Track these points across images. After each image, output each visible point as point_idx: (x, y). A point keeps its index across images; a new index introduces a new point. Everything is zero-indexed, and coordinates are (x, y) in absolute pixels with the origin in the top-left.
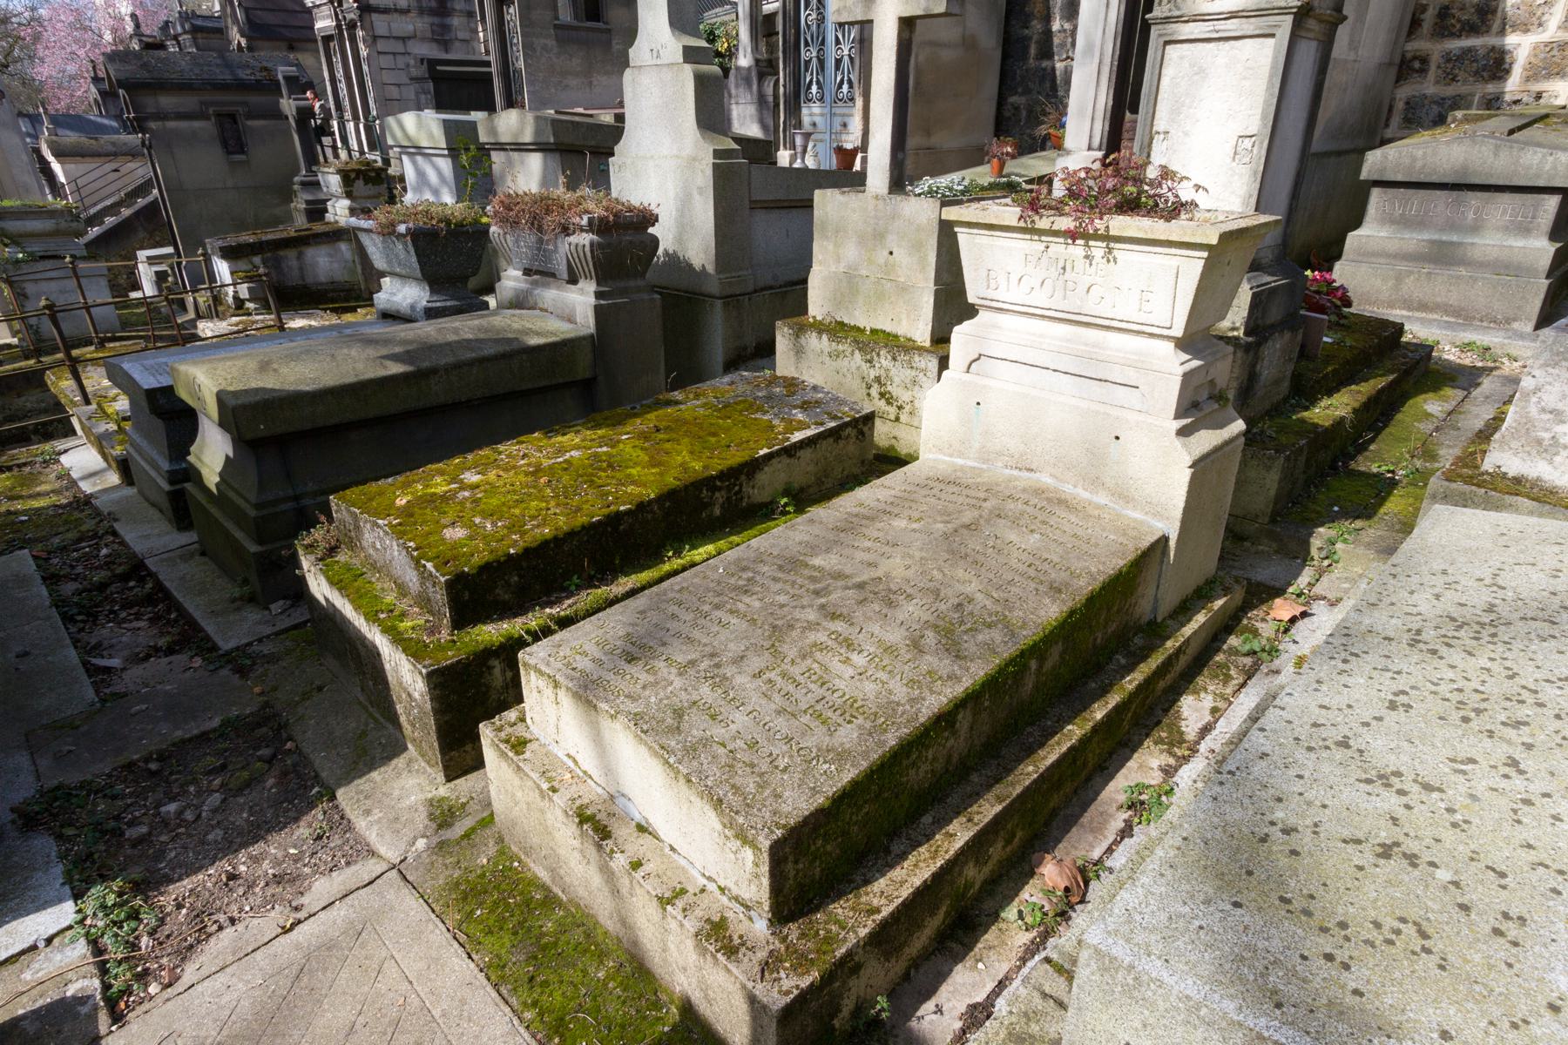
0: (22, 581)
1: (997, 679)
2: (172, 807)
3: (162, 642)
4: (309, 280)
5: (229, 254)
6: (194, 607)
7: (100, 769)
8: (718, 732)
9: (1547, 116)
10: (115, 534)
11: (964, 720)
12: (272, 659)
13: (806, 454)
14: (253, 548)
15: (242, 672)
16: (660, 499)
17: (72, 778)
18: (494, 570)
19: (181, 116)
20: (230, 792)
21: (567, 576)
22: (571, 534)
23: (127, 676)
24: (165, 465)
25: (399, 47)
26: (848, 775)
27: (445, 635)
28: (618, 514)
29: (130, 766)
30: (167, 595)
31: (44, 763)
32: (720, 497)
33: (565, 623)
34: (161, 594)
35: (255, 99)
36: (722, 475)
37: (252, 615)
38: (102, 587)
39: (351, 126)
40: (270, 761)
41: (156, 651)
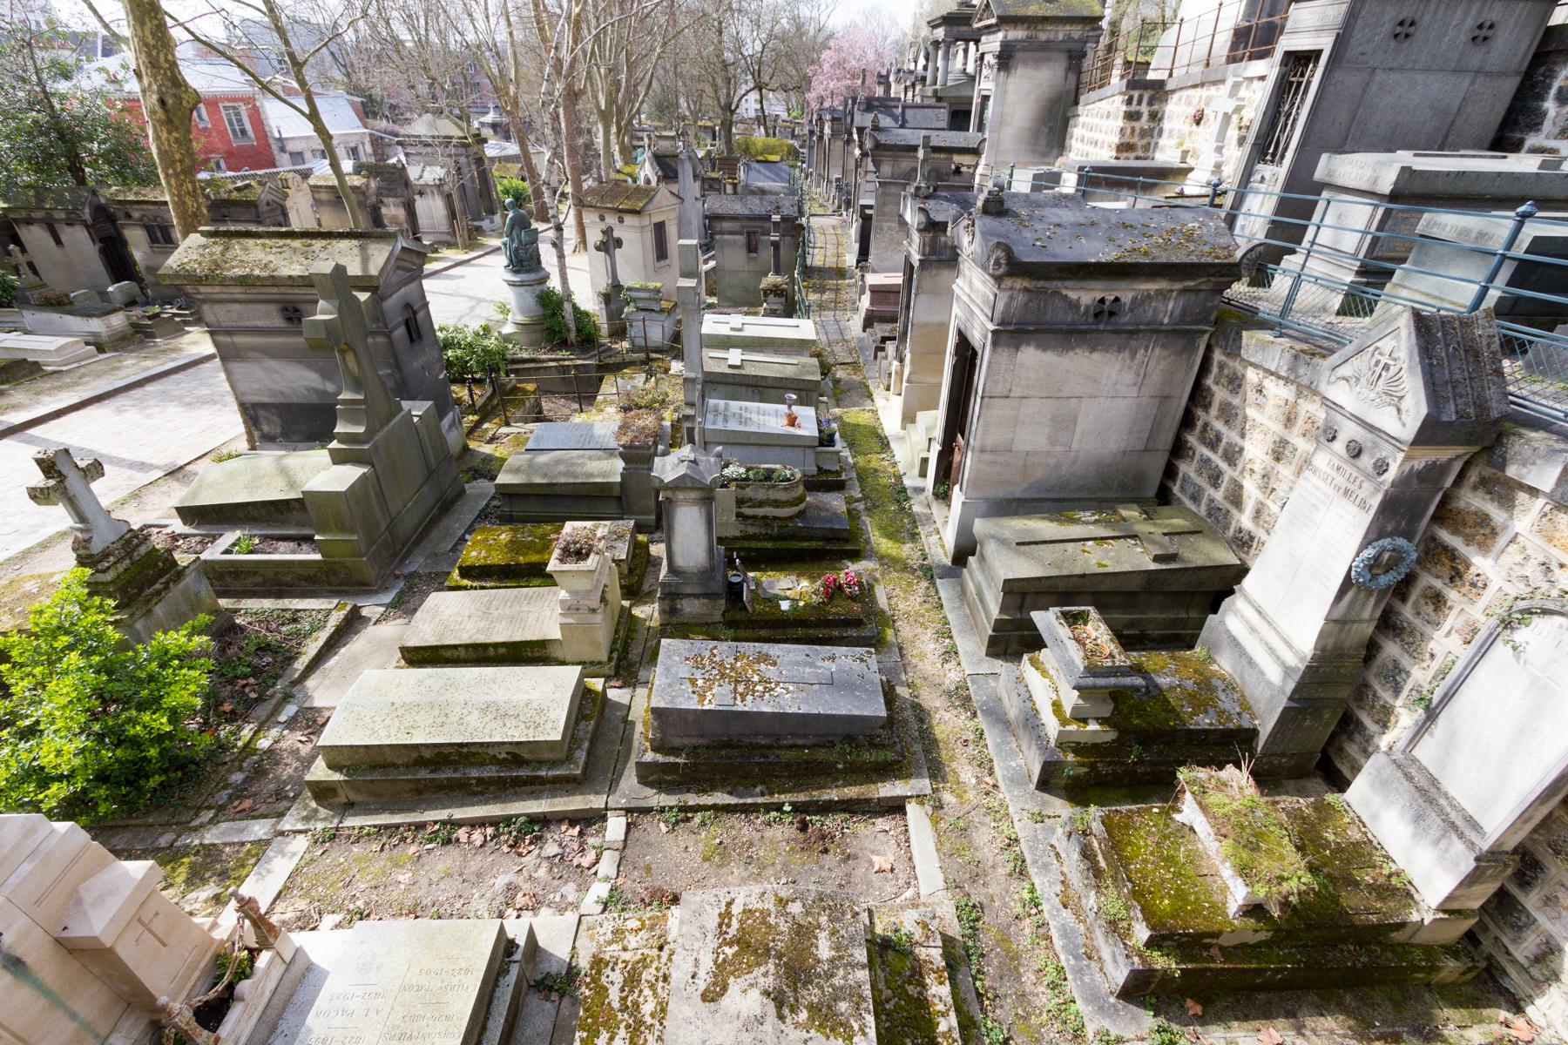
16: (526, 564)
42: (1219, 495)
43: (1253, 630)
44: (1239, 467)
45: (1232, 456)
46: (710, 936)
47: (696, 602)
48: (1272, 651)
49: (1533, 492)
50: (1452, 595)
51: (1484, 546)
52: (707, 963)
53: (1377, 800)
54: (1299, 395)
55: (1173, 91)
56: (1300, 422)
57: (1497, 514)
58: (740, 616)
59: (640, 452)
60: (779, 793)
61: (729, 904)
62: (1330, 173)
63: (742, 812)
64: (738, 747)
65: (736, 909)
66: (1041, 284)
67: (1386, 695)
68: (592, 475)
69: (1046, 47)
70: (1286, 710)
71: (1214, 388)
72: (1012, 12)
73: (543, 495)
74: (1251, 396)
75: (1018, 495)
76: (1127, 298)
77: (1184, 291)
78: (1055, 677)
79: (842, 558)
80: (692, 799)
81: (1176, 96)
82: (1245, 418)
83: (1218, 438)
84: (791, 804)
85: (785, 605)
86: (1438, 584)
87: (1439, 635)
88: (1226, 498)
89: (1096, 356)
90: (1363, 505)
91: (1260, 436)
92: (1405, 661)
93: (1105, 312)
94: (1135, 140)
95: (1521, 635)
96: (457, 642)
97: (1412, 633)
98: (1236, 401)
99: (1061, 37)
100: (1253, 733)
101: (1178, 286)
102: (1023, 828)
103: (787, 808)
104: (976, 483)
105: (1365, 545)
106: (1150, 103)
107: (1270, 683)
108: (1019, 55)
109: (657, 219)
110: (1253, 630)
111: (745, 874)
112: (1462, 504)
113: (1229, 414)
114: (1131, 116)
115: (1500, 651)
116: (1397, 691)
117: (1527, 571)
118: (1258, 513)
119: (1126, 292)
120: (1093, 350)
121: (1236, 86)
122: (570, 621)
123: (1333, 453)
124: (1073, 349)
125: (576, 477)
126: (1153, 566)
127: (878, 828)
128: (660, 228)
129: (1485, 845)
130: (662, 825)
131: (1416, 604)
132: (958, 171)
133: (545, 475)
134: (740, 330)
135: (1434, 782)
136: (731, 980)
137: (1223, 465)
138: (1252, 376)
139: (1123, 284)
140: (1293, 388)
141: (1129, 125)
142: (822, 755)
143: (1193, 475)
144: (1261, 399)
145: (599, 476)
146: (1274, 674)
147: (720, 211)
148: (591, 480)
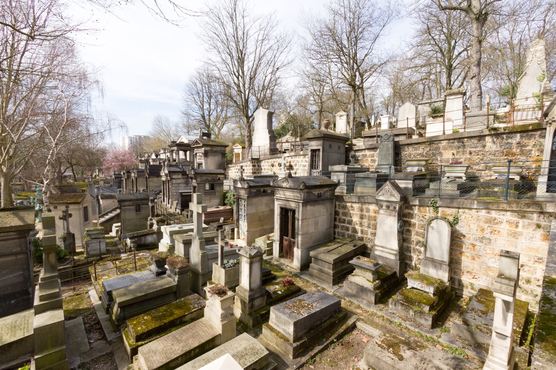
0: (80, 324)
1: (544, 295)
2: (97, 366)
3: (100, 338)
4: (146, 242)
5: (130, 238)
6: (106, 331)
7: (88, 360)
8: (152, 359)
9: (328, 252)
10: (96, 313)
11: (180, 359)
12: (115, 342)
13: (195, 313)
14: (116, 323)
15: (110, 345)
16: (168, 322)
17: (85, 361)
18: (142, 334)
19: (128, 206)
20: (104, 364)
21: (153, 334)
22: (154, 329)
23: (94, 344)
24: (107, 303)
25: (177, 185)
26: (162, 364)
27: (134, 343)
28: (161, 325)
29: (92, 360)
30: (102, 328)
31: (82, 358)
32: (178, 321)
33: (150, 342)
34: (101, 328)
35: (144, 202)
36: (179, 318)
37: (114, 334)
38: (92, 326)
39: (165, 198)
40: (110, 360)
41: (99, 339)
42: (350, 232)
43: (383, 251)
44: (353, 224)
45: (350, 222)
46: (384, 351)
47: (259, 300)
48: (390, 253)
49: (415, 206)
50: (411, 228)
51: (412, 218)
52: (392, 356)
53: (426, 269)
54: (362, 205)
55: (262, 160)
56: (365, 210)
57: (411, 212)
58: (271, 300)
59: (186, 269)
60: (330, 337)
61: (377, 343)
62: (332, 169)
63: (325, 349)
64: (314, 328)
65: (380, 343)
66: (309, 190)
67: (409, 254)
68: (162, 286)
69: (216, 152)
70: (400, 263)
71: (339, 210)
72: (206, 143)
73: (140, 302)
74: (350, 209)
75: (311, 246)
76: (322, 192)
77: (330, 190)
78: (362, 275)
79: (272, 280)
80: (312, 353)
81: (263, 161)
82: (350, 214)
83: (344, 220)
84: (335, 338)
85: (280, 292)
86: (407, 228)
87: (412, 237)
88: (352, 232)
89: (319, 206)
90: (394, 216)
91: (356, 216)
92: (409, 245)
93: (319, 196)
94: (256, 171)
95: (431, 225)
96: (175, 356)
97: (407, 239)
98: (346, 211)
99: (219, 150)
100: (395, 273)
101: (329, 189)
102: (380, 313)
103: (335, 340)
104: (302, 244)
105: (398, 223)
106: (257, 163)
107: (393, 260)
108: (209, 154)
109: (85, 205)
110: (383, 251)
111: (344, 363)
112: (404, 212)
113: (345, 214)
114: (254, 166)
115: (430, 229)
116: (410, 252)
117: (421, 219)
118: (362, 232)
119: (322, 191)
120: (319, 205)
121: (285, 158)
122: (226, 322)
123: (383, 209)
124: (315, 205)
125: (156, 288)
126: (354, 248)
127: (356, 334)
128: (86, 209)
129: (447, 264)
130: (311, 366)
131: (406, 234)
132: (219, 179)
133: (141, 292)
134: (182, 228)
135: (433, 259)
136: (400, 353)
137: (348, 225)
138: (349, 205)
139: (321, 189)
140: (360, 204)
141: (254, 168)
142: (332, 320)
143: (340, 231)
144: (353, 209)
145: (166, 285)
146: (393, 257)
147: (124, 199)
148: (164, 287)
